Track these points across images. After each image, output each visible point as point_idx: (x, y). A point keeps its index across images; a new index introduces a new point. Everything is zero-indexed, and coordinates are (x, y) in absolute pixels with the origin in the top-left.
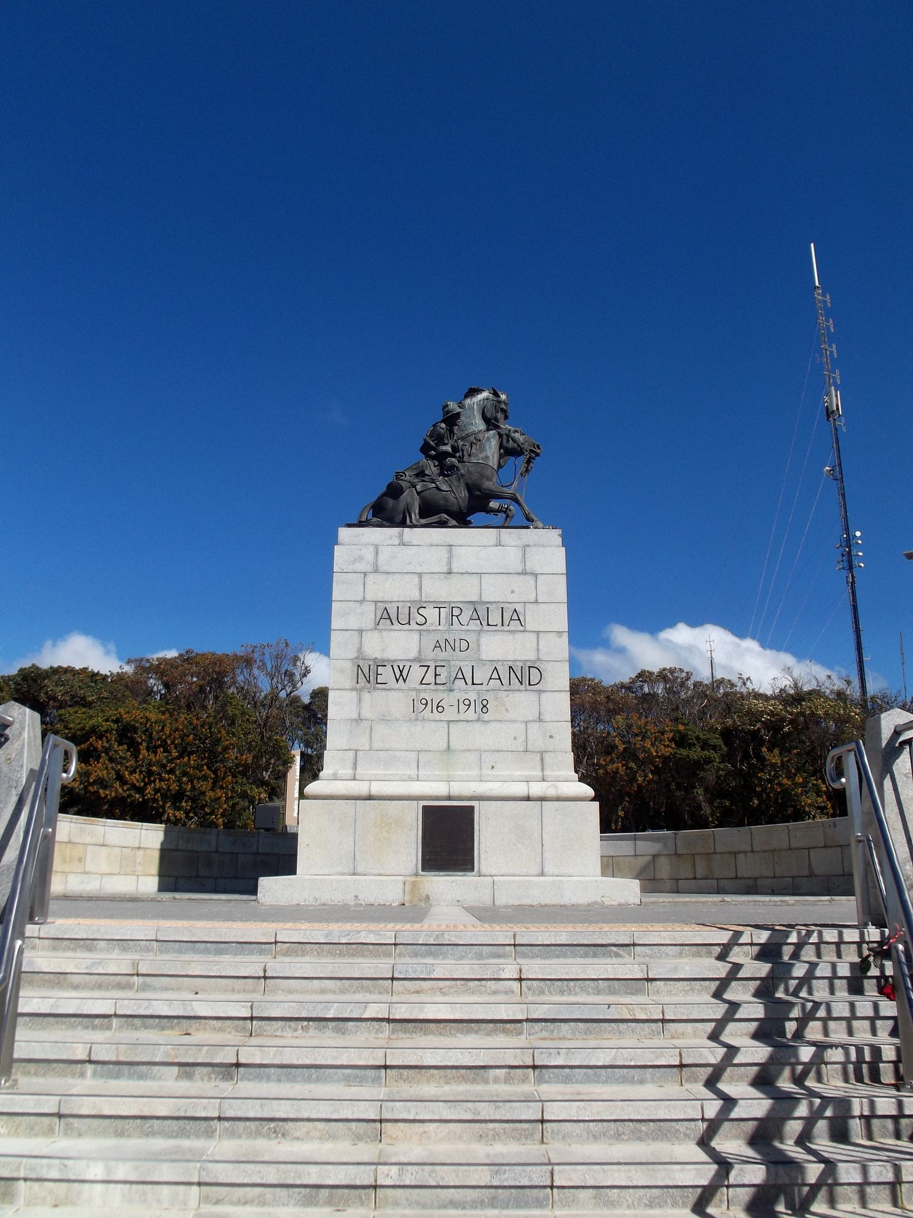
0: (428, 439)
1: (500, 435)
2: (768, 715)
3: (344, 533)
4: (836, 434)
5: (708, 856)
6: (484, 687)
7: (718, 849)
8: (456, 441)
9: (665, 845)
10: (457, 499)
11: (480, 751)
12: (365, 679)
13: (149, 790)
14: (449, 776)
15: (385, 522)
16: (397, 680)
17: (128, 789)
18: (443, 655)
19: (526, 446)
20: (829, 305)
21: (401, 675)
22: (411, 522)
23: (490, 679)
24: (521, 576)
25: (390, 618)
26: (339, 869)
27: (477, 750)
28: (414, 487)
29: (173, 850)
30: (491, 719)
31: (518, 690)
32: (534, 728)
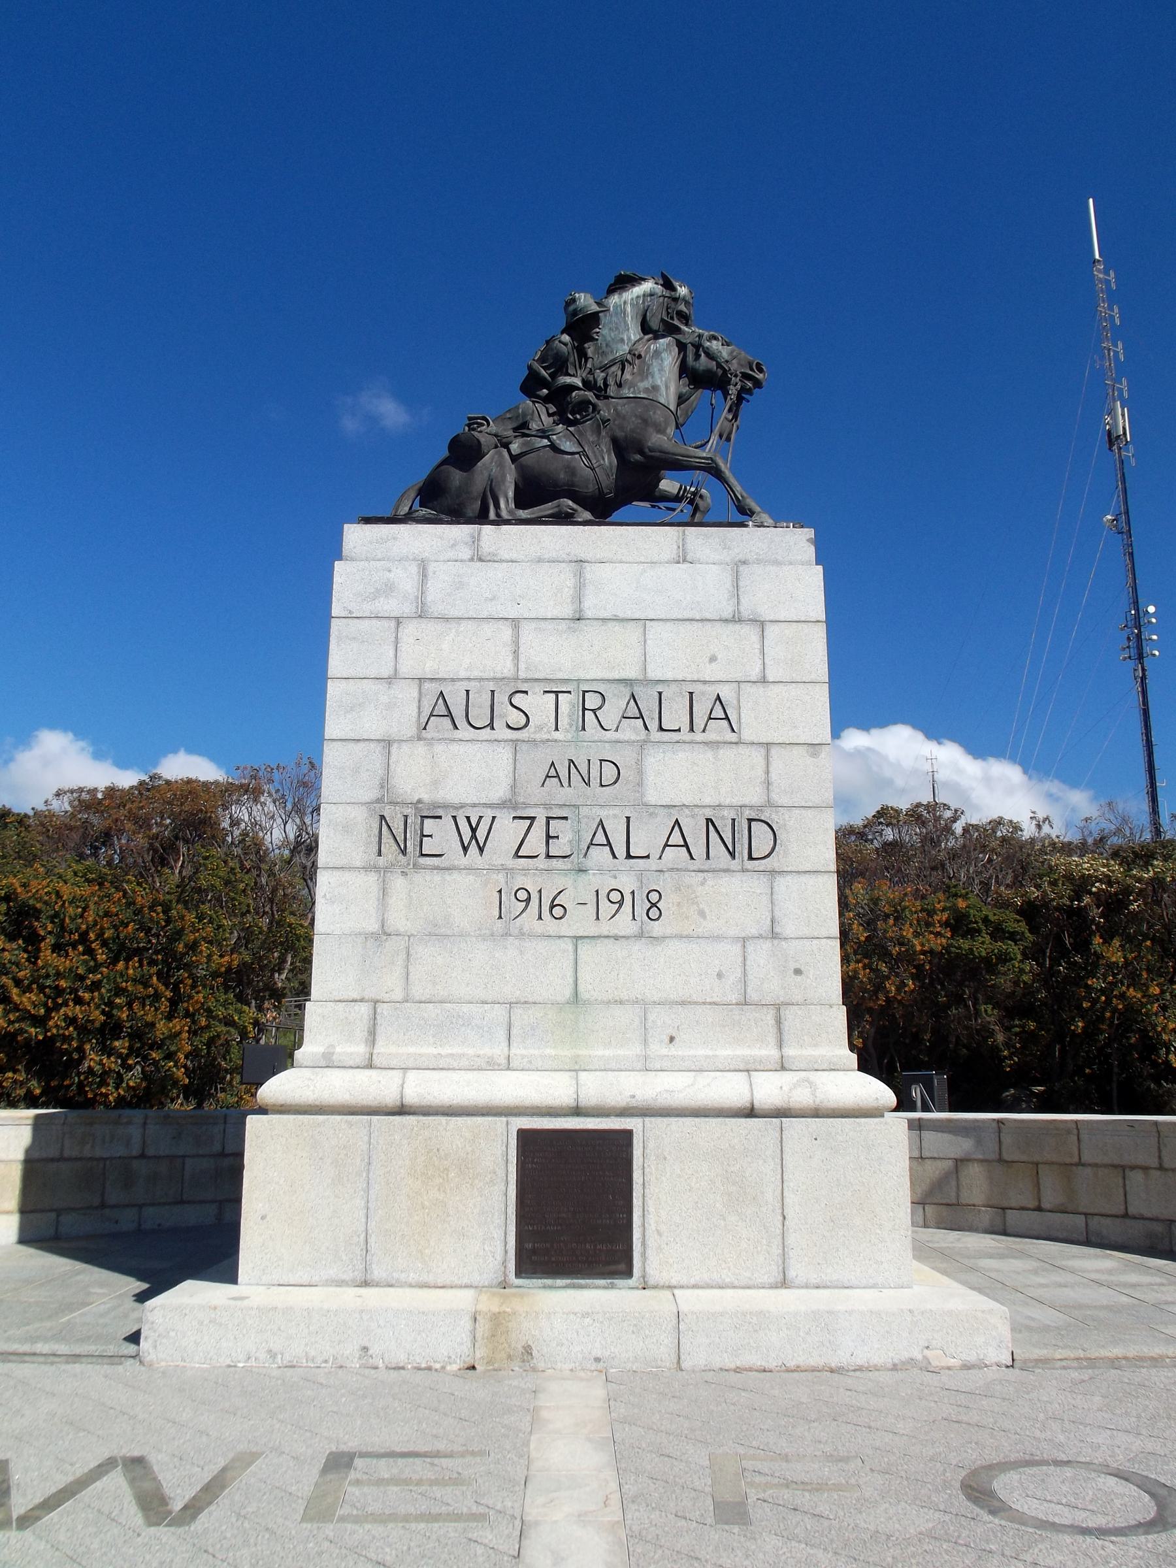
0: (536, 366)
1: (682, 347)
2: (1100, 881)
3: (356, 536)
4: (1122, 469)
5: (1068, 1169)
6: (652, 863)
7: (1086, 1158)
8: (591, 372)
9: (979, 1142)
10: (593, 469)
11: (644, 1004)
12: (395, 847)
13: (57, 1019)
14: (576, 1059)
15: (443, 516)
16: (465, 849)
17: (19, 1020)
18: (565, 794)
19: (734, 366)
20: (1114, 287)
21: (474, 836)
22: (498, 515)
23: (666, 845)
24: (730, 626)
25: (450, 715)
26: (333, 1272)
27: (636, 1002)
28: (506, 446)
29: (52, 1160)
30: (668, 932)
31: (727, 871)
32: (760, 953)
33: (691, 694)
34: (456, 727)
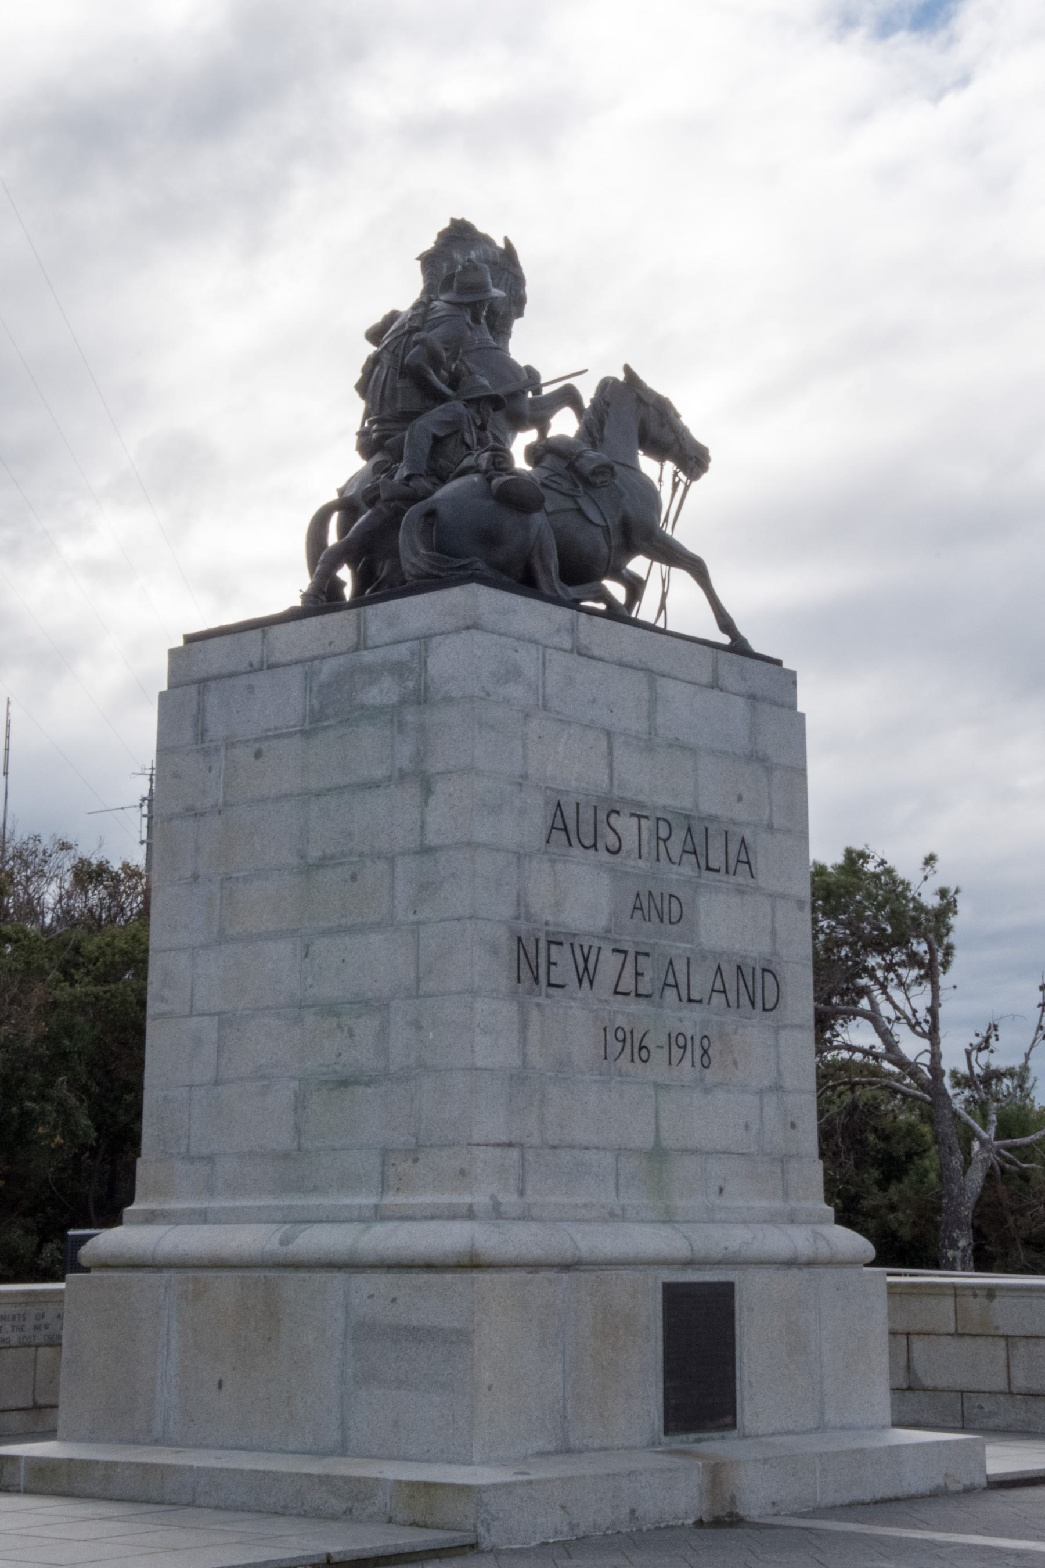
16: (580, 981)
21: (586, 969)
33: (726, 833)
34: (570, 845)
